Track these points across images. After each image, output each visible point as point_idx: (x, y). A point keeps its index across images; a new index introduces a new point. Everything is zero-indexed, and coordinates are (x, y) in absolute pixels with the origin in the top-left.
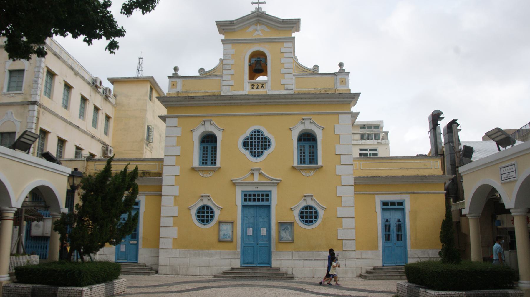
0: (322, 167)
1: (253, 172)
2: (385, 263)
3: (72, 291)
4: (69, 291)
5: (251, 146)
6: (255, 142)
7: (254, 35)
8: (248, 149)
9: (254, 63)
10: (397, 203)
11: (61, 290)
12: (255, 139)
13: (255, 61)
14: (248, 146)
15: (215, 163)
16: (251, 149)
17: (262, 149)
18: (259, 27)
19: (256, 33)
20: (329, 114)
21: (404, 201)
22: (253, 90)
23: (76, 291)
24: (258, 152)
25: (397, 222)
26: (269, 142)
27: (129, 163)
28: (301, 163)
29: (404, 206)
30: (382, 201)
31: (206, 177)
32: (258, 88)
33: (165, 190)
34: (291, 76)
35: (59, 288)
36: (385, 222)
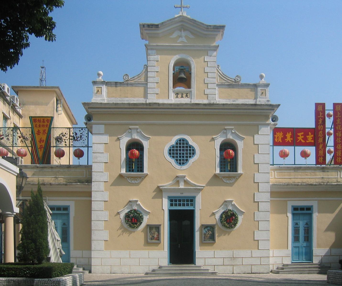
1: (178, 179)
2: (293, 260)
3: (49, 282)
4: (46, 282)
5: (177, 154)
6: (180, 150)
7: (178, 41)
8: (173, 157)
9: (178, 71)
10: (306, 208)
11: (38, 282)
12: (180, 147)
13: (179, 69)
14: (173, 154)
15: (142, 171)
16: (177, 157)
17: (187, 157)
18: (183, 34)
19: (180, 40)
20: (168, 125)
21: (69, 206)
22: (177, 99)
23: (53, 282)
24: (183, 160)
25: (63, 225)
26: (193, 150)
27: (181, 167)
28: (130, 171)
29: (69, 212)
30: (292, 206)
31: (229, 184)
32: (182, 97)
33: (95, 196)
34: (215, 86)
35: (36, 279)
36: (63, 225)
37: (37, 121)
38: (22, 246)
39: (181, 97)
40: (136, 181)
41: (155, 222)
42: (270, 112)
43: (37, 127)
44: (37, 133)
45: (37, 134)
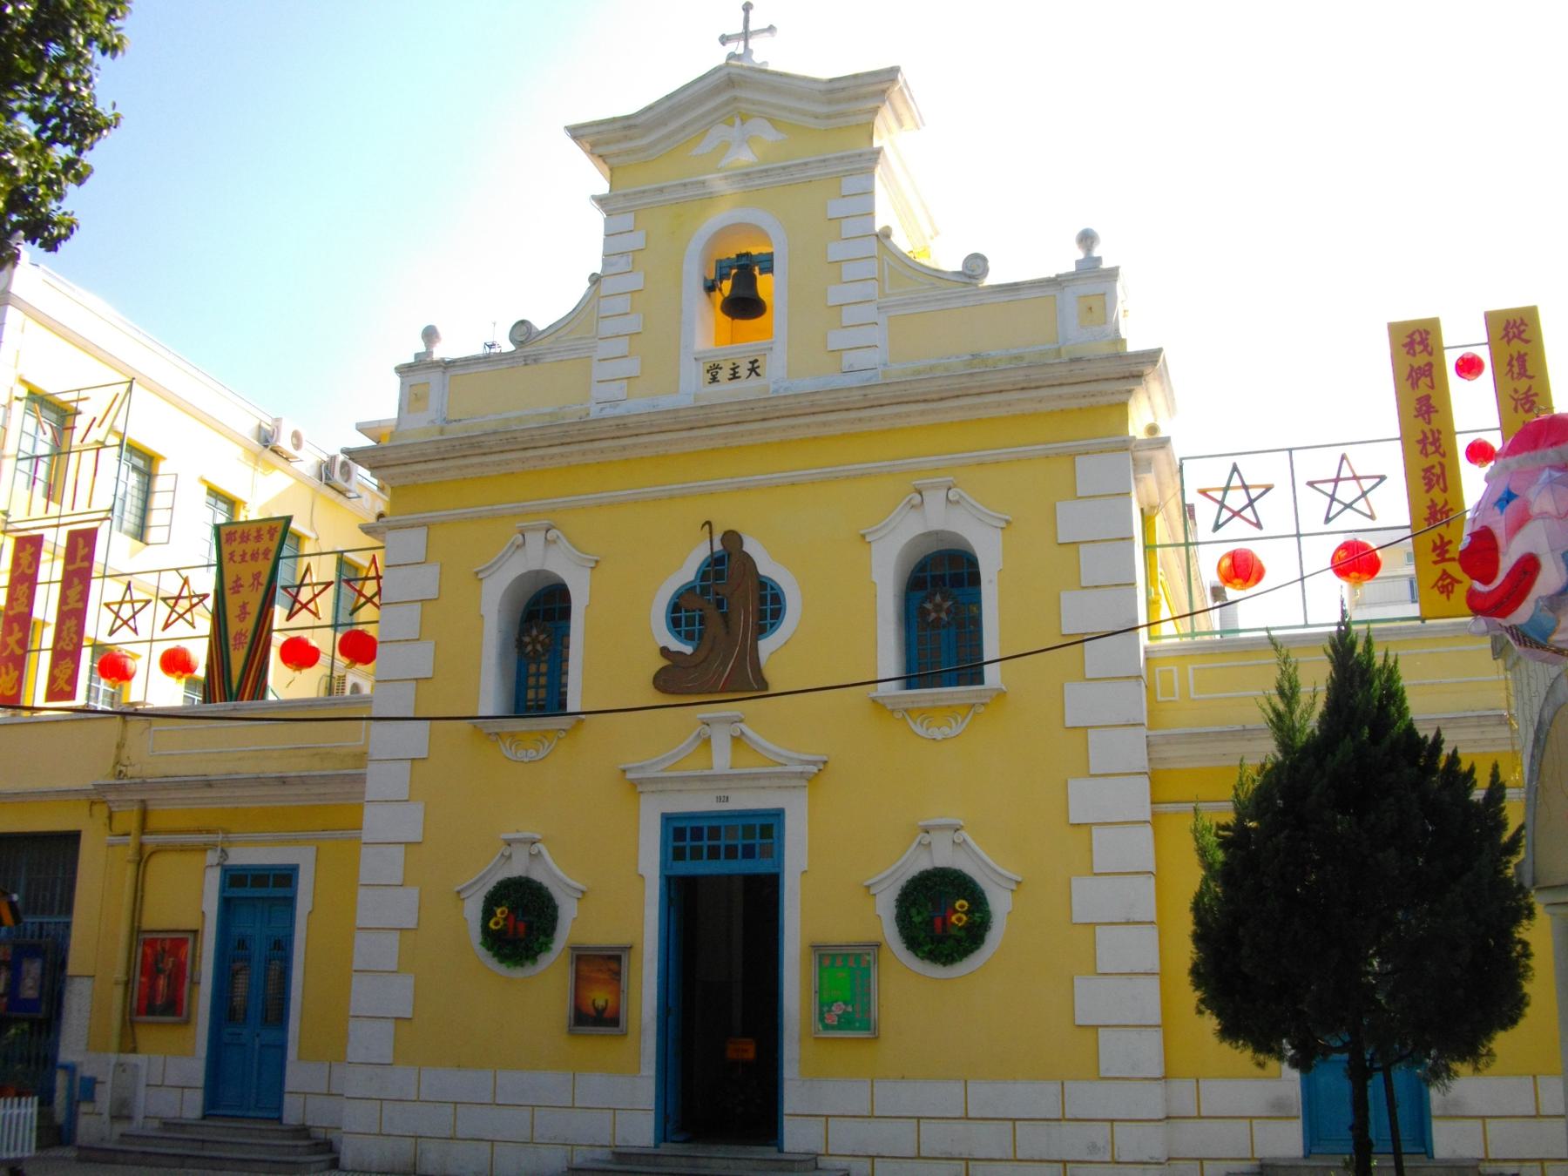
0: (1001, 694)
37: (239, 540)
38: (11, 96)
39: (730, 379)
40: (947, 730)
41: (600, 936)
42: (1128, 388)
43: (234, 562)
44: (233, 588)
45: (232, 591)
